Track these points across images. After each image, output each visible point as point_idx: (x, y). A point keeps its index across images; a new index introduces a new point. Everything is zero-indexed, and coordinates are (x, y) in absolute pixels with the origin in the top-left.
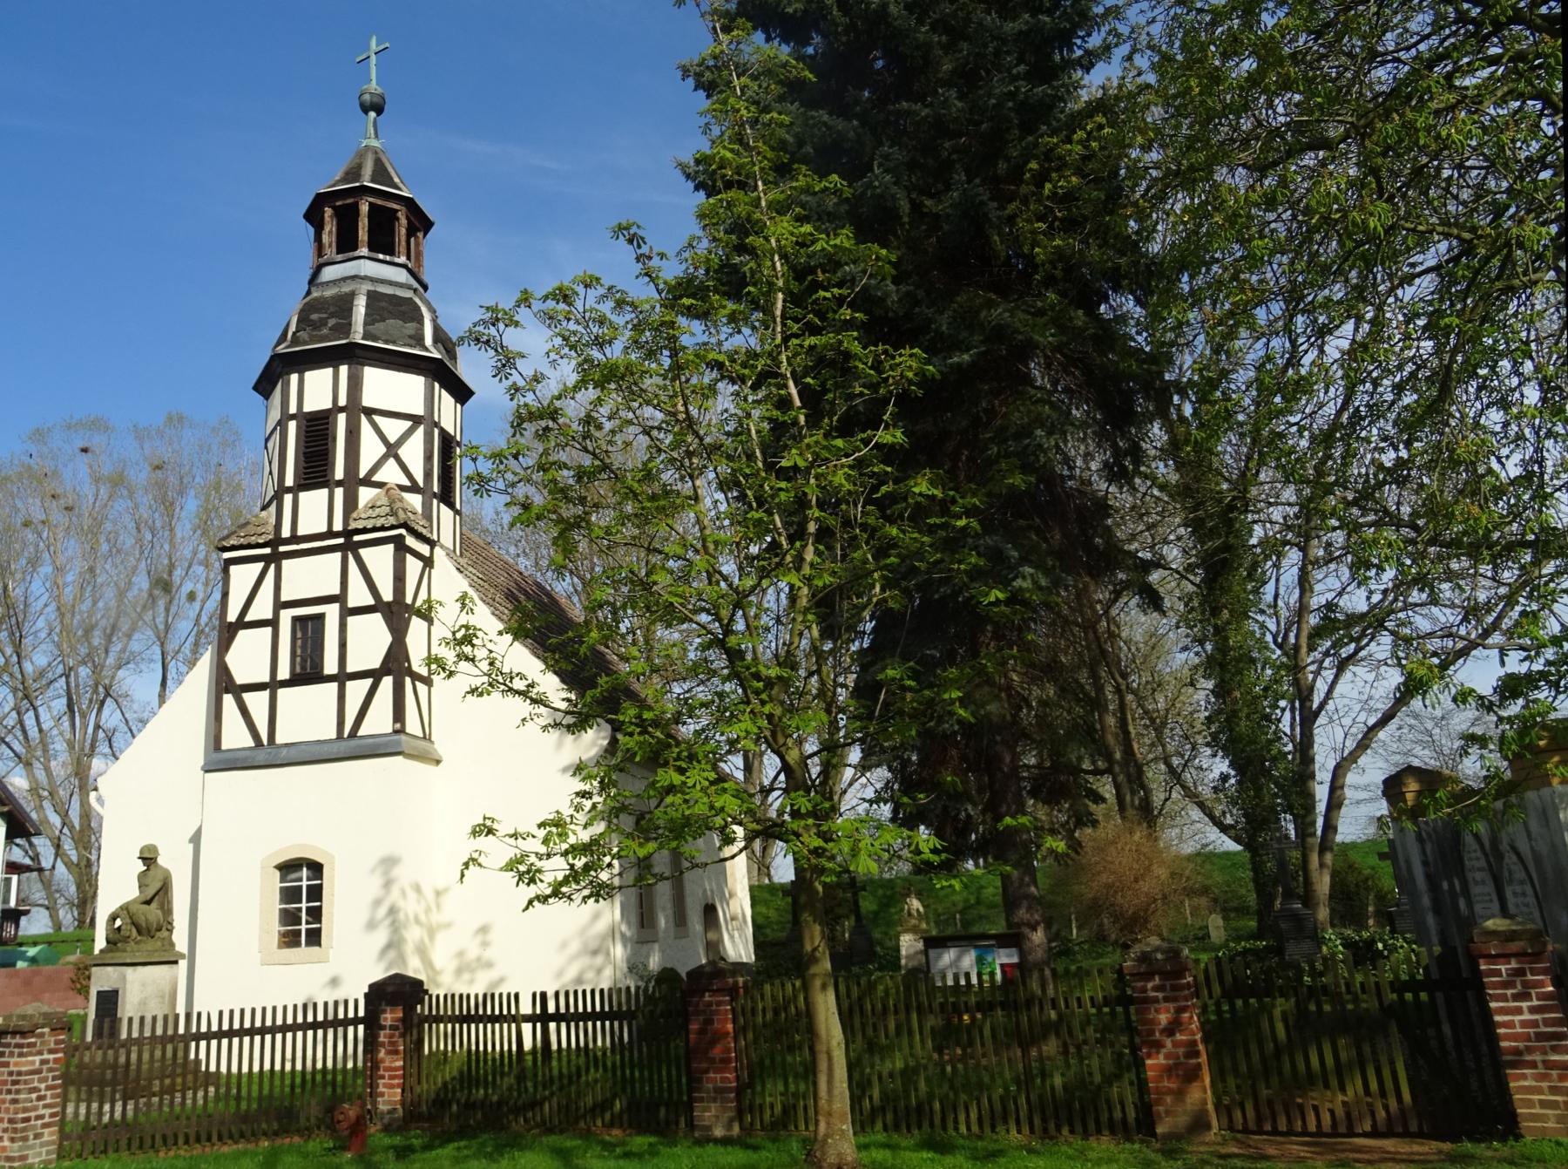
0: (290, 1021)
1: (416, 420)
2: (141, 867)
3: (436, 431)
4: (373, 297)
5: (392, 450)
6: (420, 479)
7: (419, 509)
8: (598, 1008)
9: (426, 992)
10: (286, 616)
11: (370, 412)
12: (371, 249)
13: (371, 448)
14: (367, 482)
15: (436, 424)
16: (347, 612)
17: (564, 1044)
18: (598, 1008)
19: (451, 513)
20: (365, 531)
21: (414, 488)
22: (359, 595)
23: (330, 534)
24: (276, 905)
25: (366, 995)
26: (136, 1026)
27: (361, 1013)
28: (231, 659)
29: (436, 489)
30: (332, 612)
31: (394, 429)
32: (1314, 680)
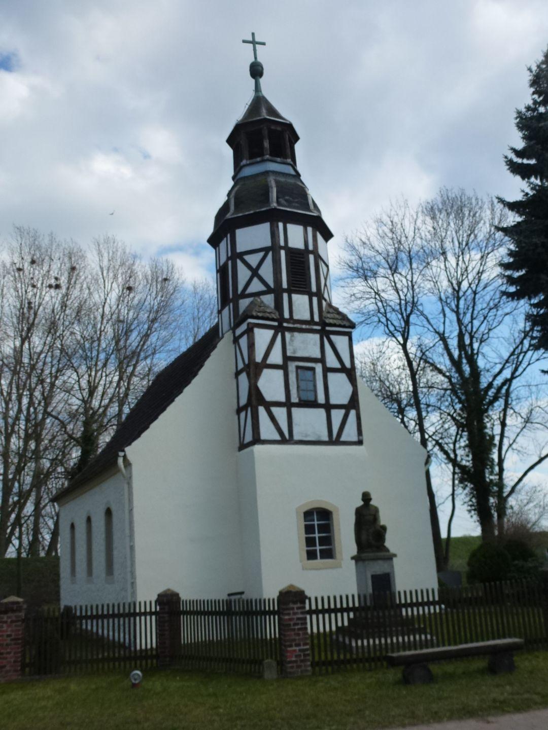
0: (431, 599)
1: (266, 250)
2: (361, 503)
3: (283, 253)
4: (278, 184)
6: (271, 284)
7: (272, 305)
8: (268, 617)
9: (306, 597)
10: (292, 366)
11: (241, 256)
12: (271, 155)
13: (267, 271)
14: (244, 295)
16: (327, 370)
17: (273, 636)
18: (268, 617)
20: (335, 325)
21: (269, 291)
22: (332, 361)
23: (311, 322)
24: (303, 536)
25: (278, 597)
26: (105, 608)
27: (437, 598)
28: (349, 389)
30: (319, 368)
31: (253, 260)
32: (454, 469)
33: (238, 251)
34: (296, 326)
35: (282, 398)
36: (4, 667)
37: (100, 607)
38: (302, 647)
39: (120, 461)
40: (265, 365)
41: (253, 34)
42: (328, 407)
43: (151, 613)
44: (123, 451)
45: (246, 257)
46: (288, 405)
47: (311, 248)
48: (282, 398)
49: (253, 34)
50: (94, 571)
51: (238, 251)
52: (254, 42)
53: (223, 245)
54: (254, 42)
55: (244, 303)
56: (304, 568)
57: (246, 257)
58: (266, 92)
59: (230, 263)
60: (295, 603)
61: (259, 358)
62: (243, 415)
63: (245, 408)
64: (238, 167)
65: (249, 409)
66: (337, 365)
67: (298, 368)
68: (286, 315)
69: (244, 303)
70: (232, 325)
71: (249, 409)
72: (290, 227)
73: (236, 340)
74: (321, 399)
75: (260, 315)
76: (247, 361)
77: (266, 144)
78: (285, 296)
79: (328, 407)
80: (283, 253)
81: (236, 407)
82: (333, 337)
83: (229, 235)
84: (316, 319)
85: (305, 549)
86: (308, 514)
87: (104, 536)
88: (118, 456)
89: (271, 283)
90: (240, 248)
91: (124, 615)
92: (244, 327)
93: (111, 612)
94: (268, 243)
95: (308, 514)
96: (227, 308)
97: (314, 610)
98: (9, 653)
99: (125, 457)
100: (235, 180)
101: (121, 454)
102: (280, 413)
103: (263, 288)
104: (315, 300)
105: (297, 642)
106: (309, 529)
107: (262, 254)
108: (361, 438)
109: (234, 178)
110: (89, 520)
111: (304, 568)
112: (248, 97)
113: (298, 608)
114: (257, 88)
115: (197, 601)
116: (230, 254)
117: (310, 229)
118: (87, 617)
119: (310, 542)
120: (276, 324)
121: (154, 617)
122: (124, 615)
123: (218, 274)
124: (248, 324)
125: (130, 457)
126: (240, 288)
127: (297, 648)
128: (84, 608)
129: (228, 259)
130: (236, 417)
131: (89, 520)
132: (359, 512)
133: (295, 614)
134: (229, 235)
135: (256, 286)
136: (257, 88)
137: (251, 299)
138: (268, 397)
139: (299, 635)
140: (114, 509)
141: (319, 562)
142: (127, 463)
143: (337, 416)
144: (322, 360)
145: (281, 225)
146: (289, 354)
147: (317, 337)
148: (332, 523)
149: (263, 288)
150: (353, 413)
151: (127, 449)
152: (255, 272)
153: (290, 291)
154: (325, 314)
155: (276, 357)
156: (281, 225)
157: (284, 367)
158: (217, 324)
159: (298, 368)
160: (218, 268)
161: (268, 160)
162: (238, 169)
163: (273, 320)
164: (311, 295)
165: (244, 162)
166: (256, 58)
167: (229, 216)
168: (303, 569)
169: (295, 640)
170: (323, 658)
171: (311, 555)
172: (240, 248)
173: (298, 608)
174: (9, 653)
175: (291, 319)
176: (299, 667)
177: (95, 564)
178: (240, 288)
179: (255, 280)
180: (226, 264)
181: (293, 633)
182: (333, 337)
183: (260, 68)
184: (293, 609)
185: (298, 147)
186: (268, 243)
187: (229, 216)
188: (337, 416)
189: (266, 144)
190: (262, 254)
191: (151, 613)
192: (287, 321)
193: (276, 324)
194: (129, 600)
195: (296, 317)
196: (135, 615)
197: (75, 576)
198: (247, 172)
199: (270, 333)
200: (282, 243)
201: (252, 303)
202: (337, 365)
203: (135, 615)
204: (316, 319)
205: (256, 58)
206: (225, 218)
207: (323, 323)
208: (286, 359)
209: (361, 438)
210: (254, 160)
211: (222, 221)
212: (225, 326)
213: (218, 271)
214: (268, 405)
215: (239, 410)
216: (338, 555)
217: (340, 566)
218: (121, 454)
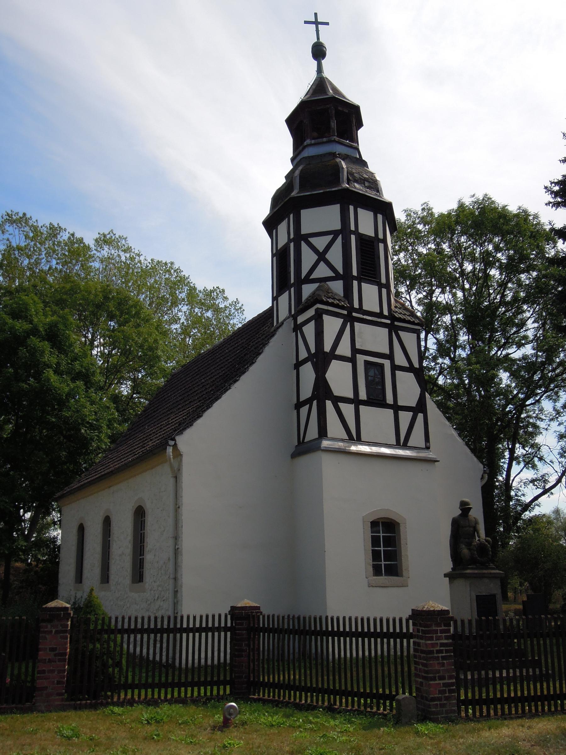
1: (336, 233)
3: (353, 237)
5: (322, 256)
10: (361, 359)
11: (306, 238)
14: (308, 280)
15: (356, 232)
16: (395, 368)
19: (375, 288)
20: (404, 321)
21: (337, 277)
22: (400, 360)
23: (380, 315)
29: (355, 273)
31: (320, 243)
33: (303, 232)
34: (365, 317)
35: (350, 395)
36: (46, 688)
37: (140, 620)
38: (446, 681)
39: (170, 450)
40: (332, 356)
41: (316, 14)
42: (396, 408)
43: (226, 629)
44: (174, 439)
45: (312, 240)
46: (356, 402)
47: (381, 236)
48: (350, 395)
49: (316, 14)
50: (112, 577)
51: (303, 232)
52: (316, 23)
53: (282, 228)
54: (316, 23)
55: (308, 290)
56: (370, 586)
57: (312, 240)
58: (327, 74)
59: (292, 245)
60: (439, 625)
61: (327, 348)
62: (304, 410)
63: (309, 401)
64: (298, 146)
65: (315, 402)
66: (406, 364)
67: (367, 363)
68: (356, 305)
69: (308, 290)
70: (293, 312)
71: (315, 402)
72: (361, 212)
73: (298, 328)
74: (390, 399)
75: (330, 301)
76: (313, 351)
77: (334, 124)
78: (355, 283)
79: (396, 408)
80: (353, 237)
81: (295, 401)
82: (400, 333)
83: (291, 216)
84: (386, 313)
85: (371, 562)
86: (374, 524)
87: (130, 537)
88: (167, 444)
89: (340, 268)
90: (305, 230)
91: (168, 631)
92: (311, 312)
93: (133, 627)
94: (338, 227)
95: (374, 524)
96: (286, 295)
97: (153, 629)
98: (52, 671)
99: (175, 446)
100: (295, 162)
101: (172, 443)
102: (348, 410)
103: (331, 274)
104: (384, 291)
105: (441, 674)
106: (375, 541)
107: (330, 237)
108: (428, 444)
109: (293, 160)
110: (107, 522)
111: (370, 586)
112: (312, 76)
113: (442, 631)
114: (320, 70)
115: (273, 616)
116: (292, 236)
117: (380, 217)
118: (122, 631)
119: (376, 555)
120: (345, 312)
121: (229, 634)
122: (168, 631)
123: (275, 258)
124: (317, 310)
125: (182, 446)
126: (304, 274)
127: (441, 682)
128: (120, 619)
129: (290, 241)
130: (295, 412)
131: (107, 522)
132: (456, 523)
133: (438, 638)
134: (291, 216)
135: (322, 271)
136: (320, 70)
137: (316, 285)
138: (337, 391)
139: (443, 665)
140: (148, 507)
141: (383, 579)
142: (178, 454)
143: (405, 417)
144: (390, 357)
145: (351, 208)
146: (358, 347)
147: (386, 331)
148: (399, 535)
149: (331, 274)
150: (420, 416)
151: (179, 439)
152: (322, 256)
153: (360, 280)
154: (393, 307)
155: (344, 349)
156: (351, 208)
157: (352, 360)
158: (270, 310)
159: (367, 363)
160: (274, 252)
161: (335, 141)
162: (298, 152)
163: (342, 308)
164: (380, 286)
165: (308, 142)
166: (318, 38)
167: (294, 194)
168: (369, 587)
169: (438, 672)
170: (484, 696)
171: (377, 571)
172: (305, 230)
173: (442, 631)
174: (52, 671)
175: (360, 310)
176: (442, 706)
177: (114, 568)
178: (304, 274)
179: (322, 264)
180: (286, 248)
181: (436, 662)
182: (400, 333)
183: (324, 49)
184: (436, 632)
185: (361, 133)
186: (338, 227)
187: (294, 194)
188: (405, 417)
189: (334, 124)
190: (330, 237)
191: (226, 629)
192: (357, 311)
193: (345, 312)
194: (170, 613)
195: (365, 308)
196: (182, 630)
197: (81, 582)
198: (307, 153)
199: (340, 321)
200: (353, 228)
201: (318, 289)
202: (406, 364)
203: (182, 630)
204: (386, 313)
205: (318, 38)
206: (290, 196)
207: (391, 317)
208: (355, 351)
209: (428, 444)
210: (320, 140)
211: (289, 198)
212: (283, 313)
213: (273, 255)
214: (337, 400)
215: (299, 405)
216: (404, 573)
217: (405, 585)
218: (172, 443)
